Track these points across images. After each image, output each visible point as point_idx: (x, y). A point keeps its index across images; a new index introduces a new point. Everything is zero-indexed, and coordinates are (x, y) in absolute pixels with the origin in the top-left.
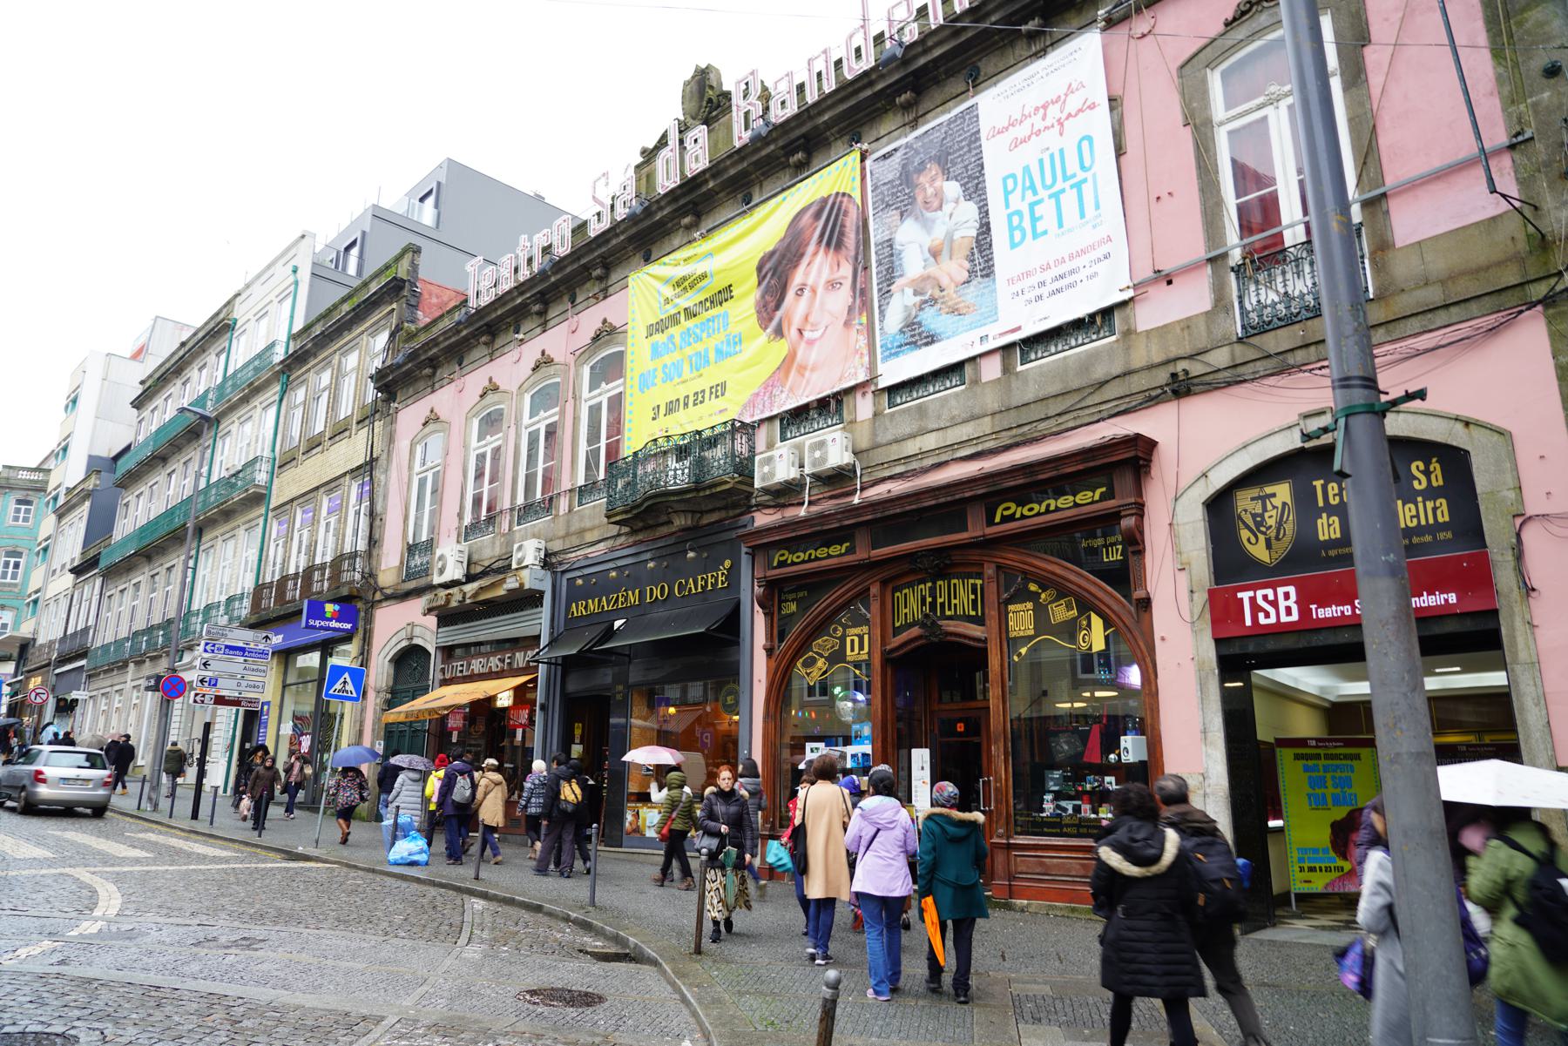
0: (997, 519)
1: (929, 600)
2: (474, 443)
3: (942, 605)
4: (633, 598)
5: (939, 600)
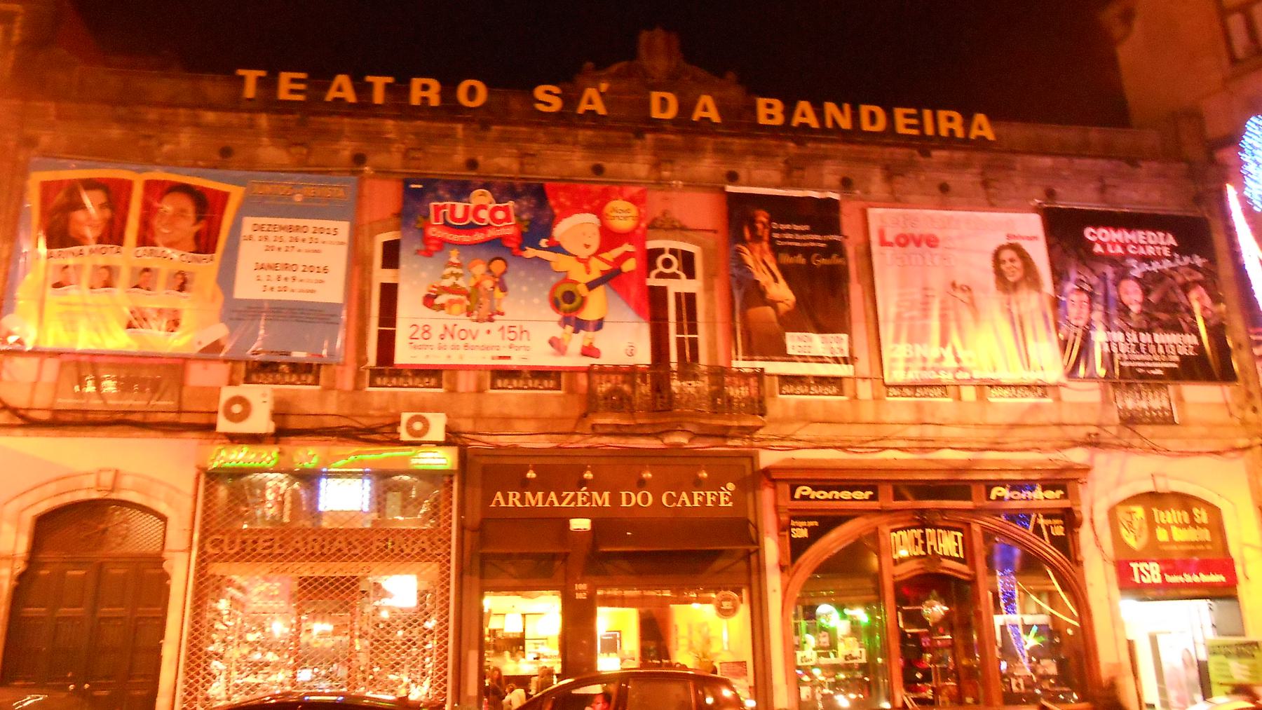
4: (603, 500)
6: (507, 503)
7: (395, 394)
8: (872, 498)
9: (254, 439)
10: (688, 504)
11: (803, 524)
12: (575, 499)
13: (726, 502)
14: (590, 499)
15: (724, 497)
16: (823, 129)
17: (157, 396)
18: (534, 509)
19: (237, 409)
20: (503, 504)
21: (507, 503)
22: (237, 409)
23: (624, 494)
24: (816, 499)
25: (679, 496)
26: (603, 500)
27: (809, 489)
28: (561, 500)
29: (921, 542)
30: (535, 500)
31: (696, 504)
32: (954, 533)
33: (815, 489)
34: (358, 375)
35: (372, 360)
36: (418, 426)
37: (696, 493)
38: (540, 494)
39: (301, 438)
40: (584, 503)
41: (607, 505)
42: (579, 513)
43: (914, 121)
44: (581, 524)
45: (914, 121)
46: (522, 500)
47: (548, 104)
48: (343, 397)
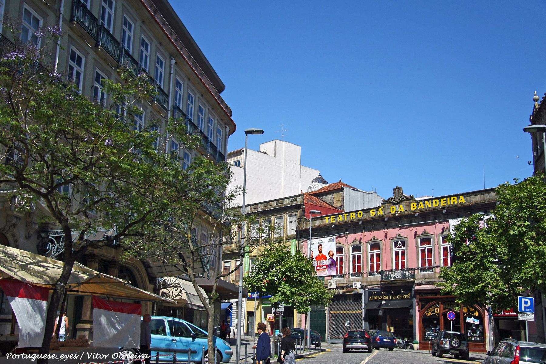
2: (369, 251)
35: (351, 272)
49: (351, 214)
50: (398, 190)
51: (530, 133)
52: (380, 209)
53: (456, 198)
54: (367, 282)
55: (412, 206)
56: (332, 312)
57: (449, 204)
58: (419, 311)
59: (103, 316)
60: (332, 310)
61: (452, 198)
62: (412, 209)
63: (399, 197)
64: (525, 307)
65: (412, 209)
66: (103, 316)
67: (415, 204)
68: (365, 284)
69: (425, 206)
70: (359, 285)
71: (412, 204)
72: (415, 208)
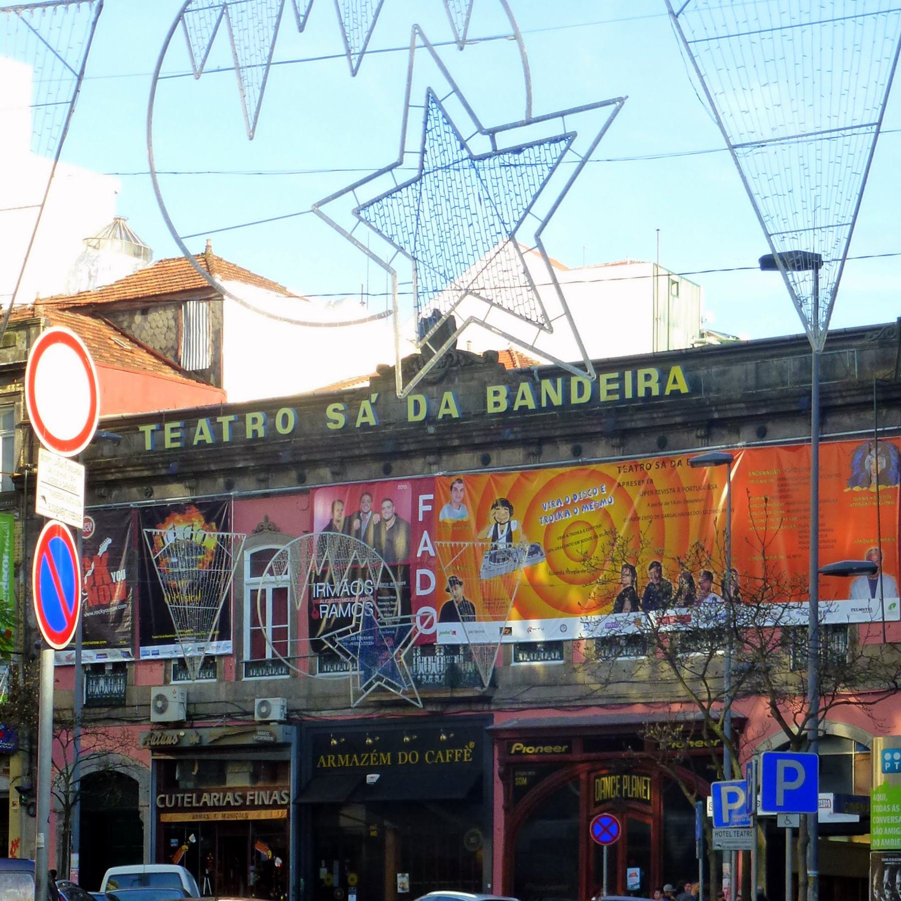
0: (513, 752)
1: (618, 786)
3: (626, 790)
4: (386, 759)
5: (624, 788)
6: (327, 764)
7: (259, 682)
8: (569, 751)
9: (178, 725)
10: (442, 761)
11: (524, 773)
12: (369, 758)
13: (468, 758)
14: (378, 758)
15: (466, 753)
16: (539, 408)
17: (298, 602)
18: (344, 768)
19: (160, 704)
20: (324, 765)
21: (327, 764)
22: (160, 704)
23: (400, 754)
24: (526, 753)
25: (436, 752)
26: (386, 759)
27: (521, 745)
28: (360, 760)
29: (618, 786)
30: (344, 760)
31: (448, 760)
32: (644, 778)
33: (526, 745)
34: (238, 667)
35: (247, 656)
36: (264, 710)
37: (448, 751)
38: (347, 756)
39: (611, 722)
40: (374, 762)
41: (389, 763)
42: (372, 770)
43: (616, 386)
44: (372, 778)
45: (616, 386)
46: (336, 761)
47: (335, 410)
48: (229, 687)
49: (249, 417)
50: (438, 329)
51: (297, 411)
52: (365, 405)
53: (654, 372)
54: (309, 697)
55: (491, 399)
56: (167, 818)
57: (629, 394)
58: (507, 810)
59: (426, 532)
60: (167, 810)
61: (641, 373)
62: (491, 409)
63: (444, 360)
64: (787, 793)
65: (491, 409)
66: (426, 532)
67: (503, 390)
68: (300, 704)
69: (538, 399)
70: (276, 713)
71: (490, 390)
72: (503, 407)
